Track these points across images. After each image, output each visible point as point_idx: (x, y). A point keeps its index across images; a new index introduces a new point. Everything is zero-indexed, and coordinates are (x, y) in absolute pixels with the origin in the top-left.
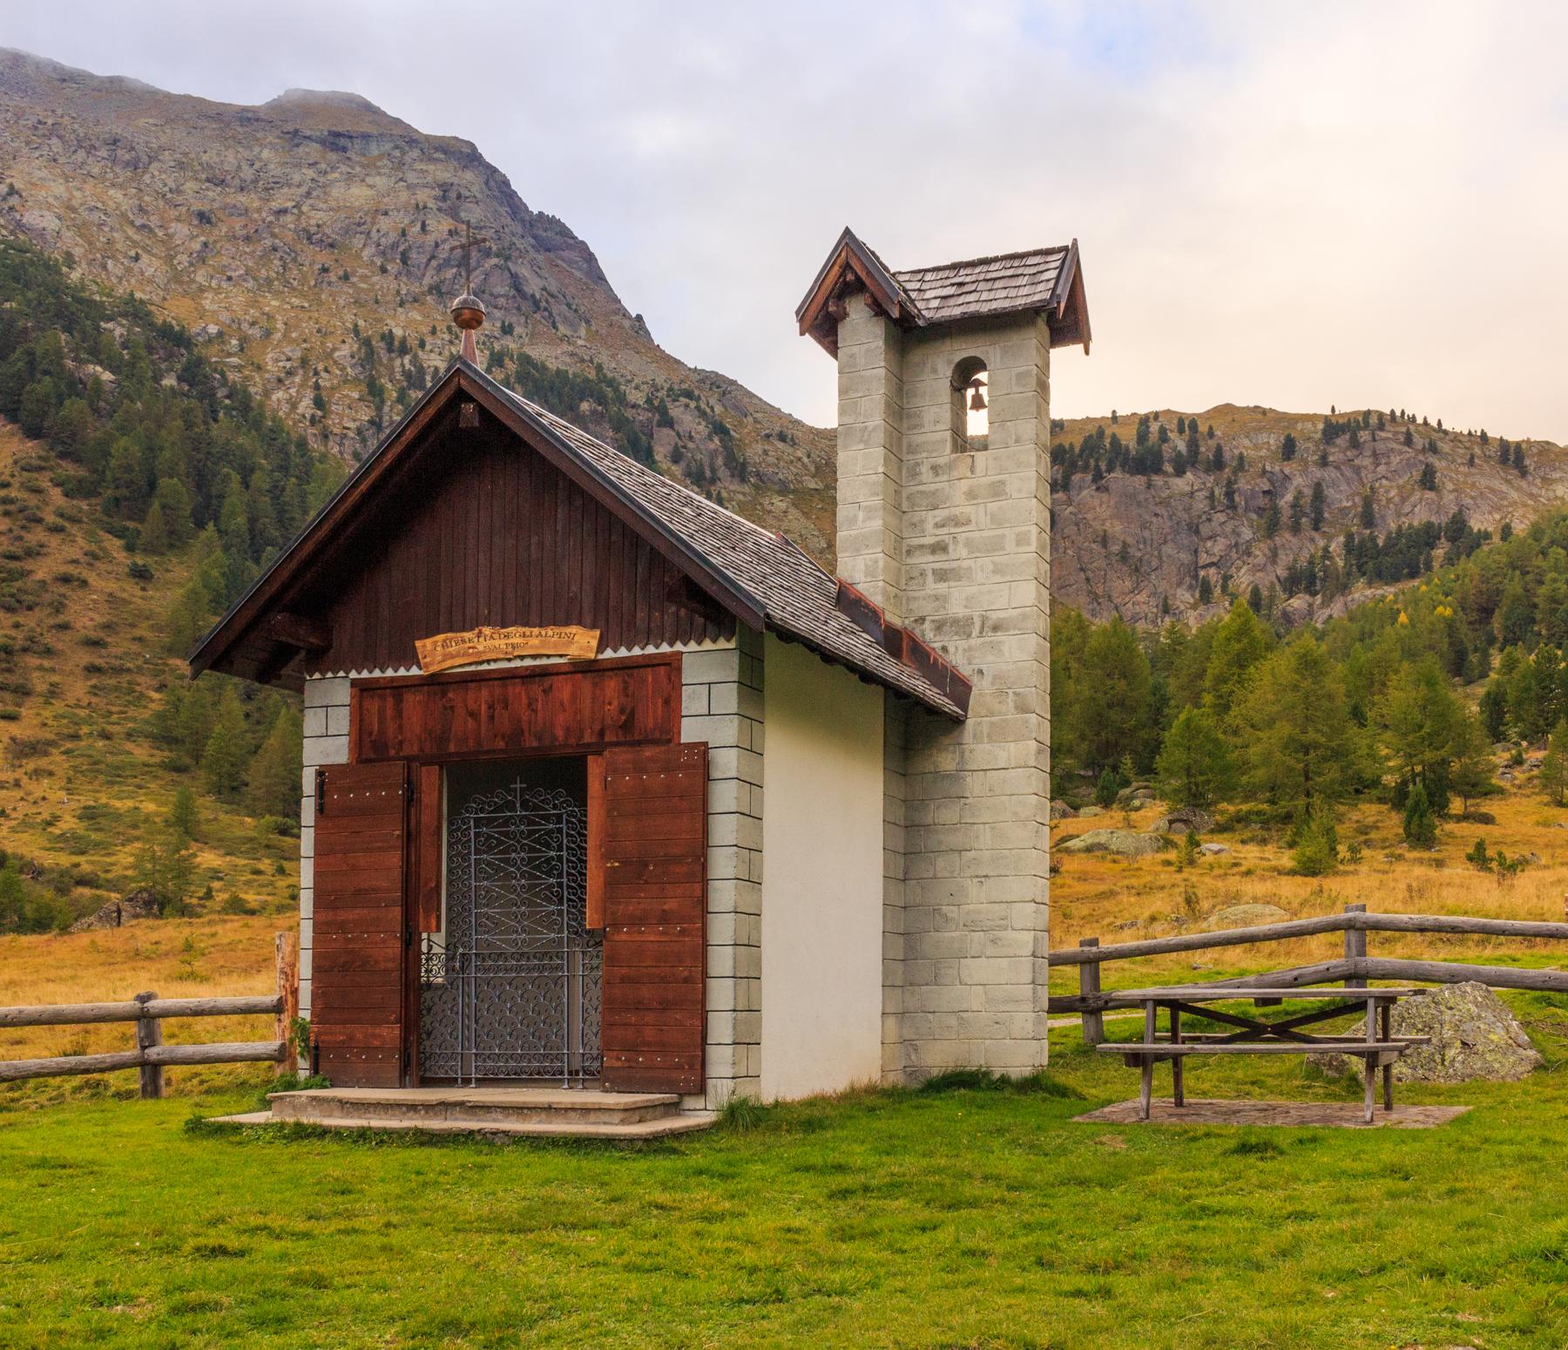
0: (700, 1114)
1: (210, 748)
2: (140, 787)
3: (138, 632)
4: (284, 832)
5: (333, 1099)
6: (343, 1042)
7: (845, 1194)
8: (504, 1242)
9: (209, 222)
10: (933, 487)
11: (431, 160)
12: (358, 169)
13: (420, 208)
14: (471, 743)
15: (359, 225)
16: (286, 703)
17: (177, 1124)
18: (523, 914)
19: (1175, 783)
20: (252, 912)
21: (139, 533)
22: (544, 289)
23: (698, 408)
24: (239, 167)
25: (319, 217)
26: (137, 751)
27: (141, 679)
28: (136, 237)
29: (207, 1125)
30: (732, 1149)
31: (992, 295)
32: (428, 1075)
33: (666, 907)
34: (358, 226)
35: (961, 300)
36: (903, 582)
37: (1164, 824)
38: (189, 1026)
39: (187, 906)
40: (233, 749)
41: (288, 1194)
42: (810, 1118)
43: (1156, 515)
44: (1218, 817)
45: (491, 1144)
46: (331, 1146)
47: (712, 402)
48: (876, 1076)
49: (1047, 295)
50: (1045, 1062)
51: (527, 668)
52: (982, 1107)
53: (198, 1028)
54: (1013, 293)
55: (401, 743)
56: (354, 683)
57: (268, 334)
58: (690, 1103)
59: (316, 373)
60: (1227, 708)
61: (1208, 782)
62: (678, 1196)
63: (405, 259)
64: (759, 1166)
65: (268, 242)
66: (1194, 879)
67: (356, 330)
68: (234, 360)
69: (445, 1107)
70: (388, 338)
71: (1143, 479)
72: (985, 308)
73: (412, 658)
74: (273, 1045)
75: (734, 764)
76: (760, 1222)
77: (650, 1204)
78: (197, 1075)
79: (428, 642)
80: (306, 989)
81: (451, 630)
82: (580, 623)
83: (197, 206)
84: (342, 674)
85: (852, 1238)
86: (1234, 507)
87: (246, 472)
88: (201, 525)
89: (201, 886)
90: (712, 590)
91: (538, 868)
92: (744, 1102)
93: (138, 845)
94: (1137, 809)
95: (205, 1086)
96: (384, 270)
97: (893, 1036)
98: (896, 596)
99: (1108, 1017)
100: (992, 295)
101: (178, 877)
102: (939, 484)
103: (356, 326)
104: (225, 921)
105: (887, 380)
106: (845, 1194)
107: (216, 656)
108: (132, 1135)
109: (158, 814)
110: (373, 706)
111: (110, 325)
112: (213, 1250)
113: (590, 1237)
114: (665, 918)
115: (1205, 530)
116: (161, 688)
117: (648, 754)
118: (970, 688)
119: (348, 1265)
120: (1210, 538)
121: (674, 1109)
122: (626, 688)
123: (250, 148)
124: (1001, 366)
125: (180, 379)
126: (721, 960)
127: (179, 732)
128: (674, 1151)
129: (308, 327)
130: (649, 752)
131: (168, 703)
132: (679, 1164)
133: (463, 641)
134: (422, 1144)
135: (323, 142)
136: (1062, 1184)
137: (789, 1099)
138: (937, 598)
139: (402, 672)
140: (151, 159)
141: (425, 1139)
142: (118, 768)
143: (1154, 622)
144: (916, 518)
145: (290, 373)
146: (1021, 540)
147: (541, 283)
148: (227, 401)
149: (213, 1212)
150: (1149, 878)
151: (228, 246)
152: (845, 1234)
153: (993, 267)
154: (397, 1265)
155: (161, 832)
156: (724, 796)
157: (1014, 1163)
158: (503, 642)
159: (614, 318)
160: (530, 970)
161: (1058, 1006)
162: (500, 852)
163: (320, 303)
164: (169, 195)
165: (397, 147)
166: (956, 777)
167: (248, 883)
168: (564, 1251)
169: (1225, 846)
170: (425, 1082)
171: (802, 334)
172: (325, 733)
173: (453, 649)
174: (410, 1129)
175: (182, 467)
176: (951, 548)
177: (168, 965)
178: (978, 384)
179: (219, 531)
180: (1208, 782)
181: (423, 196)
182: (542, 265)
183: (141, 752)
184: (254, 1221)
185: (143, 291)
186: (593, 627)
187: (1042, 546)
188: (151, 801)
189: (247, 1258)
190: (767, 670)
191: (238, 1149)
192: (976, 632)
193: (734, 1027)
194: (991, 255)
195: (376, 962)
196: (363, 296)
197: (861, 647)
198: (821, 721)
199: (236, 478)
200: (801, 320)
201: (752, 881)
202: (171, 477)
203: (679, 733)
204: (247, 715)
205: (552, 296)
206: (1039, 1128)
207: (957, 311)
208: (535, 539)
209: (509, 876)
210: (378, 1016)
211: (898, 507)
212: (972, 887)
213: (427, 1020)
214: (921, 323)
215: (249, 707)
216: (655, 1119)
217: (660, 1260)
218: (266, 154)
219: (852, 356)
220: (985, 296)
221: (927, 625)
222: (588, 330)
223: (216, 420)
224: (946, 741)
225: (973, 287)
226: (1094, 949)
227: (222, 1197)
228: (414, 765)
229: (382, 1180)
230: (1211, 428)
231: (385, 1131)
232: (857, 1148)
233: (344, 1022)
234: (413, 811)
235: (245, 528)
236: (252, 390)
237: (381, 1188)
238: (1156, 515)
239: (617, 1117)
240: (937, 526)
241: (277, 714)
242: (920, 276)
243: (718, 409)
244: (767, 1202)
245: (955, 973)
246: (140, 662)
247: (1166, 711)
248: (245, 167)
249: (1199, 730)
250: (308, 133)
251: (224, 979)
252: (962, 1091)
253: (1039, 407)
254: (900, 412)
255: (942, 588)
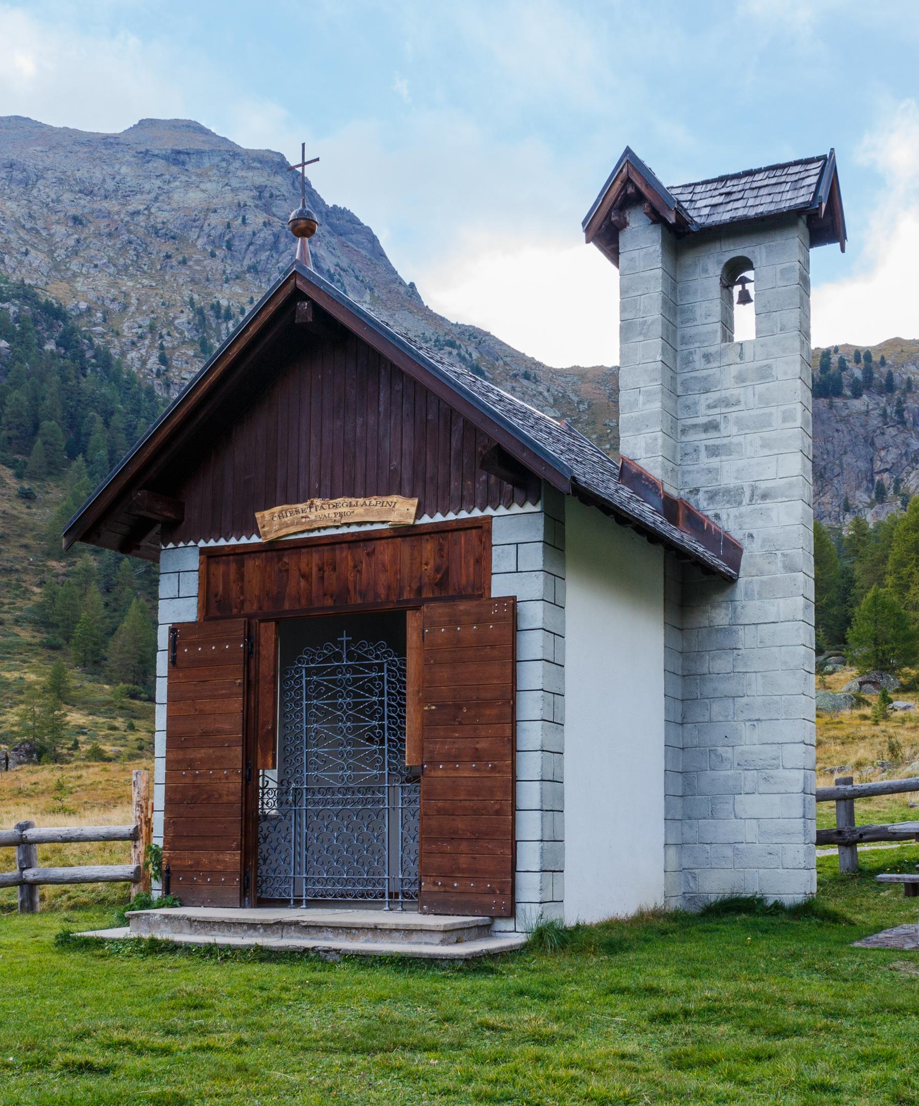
0: (510, 935)
1: (78, 632)
2: (24, 662)
3: (24, 541)
4: (134, 696)
5: (183, 917)
6: (191, 866)
7: (667, 1018)
8: (351, 1065)
9: (81, 223)
10: (704, 373)
11: (250, 168)
12: (194, 178)
13: (241, 206)
14: (303, 601)
15: (194, 221)
16: (136, 594)
17: (48, 937)
18: (349, 753)
19: (865, 650)
20: (109, 760)
21: (26, 463)
22: (337, 265)
23: (459, 355)
24: (104, 180)
25: (162, 216)
26: (23, 634)
27: (26, 578)
28: (27, 237)
29: (74, 939)
30: (544, 970)
31: (758, 201)
32: (264, 896)
33: (478, 746)
34: (194, 221)
35: (730, 206)
36: (679, 455)
37: (855, 685)
38: (60, 851)
39: (59, 755)
40: (95, 631)
41: (146, 1008)
42: (610, 940)
43: (837, 431)
44: (902, 679)
45: (324, 961)
46: (182, 960)
47: (470, 349)
48: (660, 902)
49: (810, 198)
50: (815, 890)
51: (353, 534)
52: (766, 931)
53: (67, 852)
54: (777, 198)
55: (242, 602)
56: (203, 551)
57: (125, 307)
58: (501, 925)
59: (161, 337)
60: (907, 587)
61: (893, 649)
62: (506, 1016)
63: (229, 247)
64: (574, 987)
65: (125, 237)
66: (891, 731)
67: (192, 302)
68: (99, 329)
69: (281, 926)
70: (216, 308)
71: (826, 401)
72: (752, 213)
73: (252, 527)
74: (126, 869)
75: (540, 615)
76: (591, 1047)
77: (482, 1024)
78: (66, 892)
79: (267, 513)
80: (159, 820)
81: (286, 503)
82: (400, 493)
83: (72, 211)
84: (192, 543)
85: (690, 1067)
86: (903, 422)
87: (107, 415)
88: (72, 456)
89: (70, 739)
90: (523, 457)
91: (361, 712)
92: (552, 924)
93: (23, 706)
94: (831, 673)
95: (72, 902)
96: (213, 255)
97: (673, 866)
98: (673, 470)
99: (861, 848)
100: (758, 201)
101: (52, 732)
102: (712, 369)
103: (192, 299)
104: (88, 767)
105: (664, 279)
106: (667, 1018)
107: (87, 529)
108: (10, 947)
109: (37, 683)
110: (219, 570)
111: (6, 305)
112: (80, 1066)
113: (432, 1060)
114: (477, 756)
115: (879, 442)
116: (41, 584)
117: (462, 608)
118: (741, 551)
119: (207, 1086)
120: (884, 448)
121: (485, 931)
122: (441, 550)
123: (112, 166)
124: (770, 261)
125: (58, 344)
126: (529, 795)
127: (55, 619)
128: (492, 971)
129: (155, 301)
130: (463, 606)
131: (46, 595)
132: (499, 983)
133: (297, 512)
134: (262, 960)
135: (166, 158)
136: (877, 1011)
137: (588, 923)
138: (709, 471)
139: (244, 540)
140: (38, 178)
141: (264, 955)
142: (9, 647)
143: (837, 519)
144: (689, 400)
145: (141, 337)
146: (787, 417)
147: (335, 260)
148: (93, 361)
149: (79, 1025)
150: (852, 730)
151: (95, 241)
152: (680, 1063)
153: (758, 177)
154: (253, 1087)
155: (39, 696)
156: (532, 645)
157: (818, 989)
158: (332, 511)
159: (393, 286)
160: (354, 803)
161: (823, 839)
162: (328, 698)
163: (164, 282)
164: (51, 204)
165: (224, 160)
166: (729, 630)
167: (106, 737)
168: (414, 1077)
169: (910, 703)
170: (262, 903)
171: (588, 242)
172: (178, 602)
173: (288, 519)
174: (251, 946)
175: (59, 413)
176: (722, 427)
177: (43, 802)
178: (744, 281)
179: (86, 461)
180: (893, 649)
181: (243, 197)
182: (336, 247)
183: (26, 635)
184: (118, 1036)
185: (31, 278)
186: (412, 496)
187: (805, 421)
188: (33, 672)
189: (112, 1076)
190: (567, 528)
191: (101, 962)
192: (746, 500)
193: (542, 856)
194: (755, 167)
195: (220, 796)
196: (197, 275)
197: (647, 511)
198: (614, 576)
199: (99, 419)
200: (587, 231)
201: (555, 722)
202: (51, 420)
203: (490, 588)
204: (107, 605)
205: (344, 270)
206: (830, 953)
207: (726, 217)
208: (360, 421)
209: (337, 719)
210: (223, 843)
211: (673, 391)
212: (745, 730)
213: (264, 847)
214: (694, 228)
215: (109, 598)
216: (470, 940)
217: (509, 1088)
218: (124, 170)
219: (632, 259)
220: (751, 202)
221: (701, 496)
222: (372, 296)
223: (85, 375)
224: (719, 598)
225: (740, 195)
226: (849, 787)
227: (88, 1010)
228: (255, 621)
229: (230, 995)
230: (883, 358)
231: (229, 947)
232: (664, 972)
233: (192, 849)
234: (252, 663)
235: (106, 458)
236: (112, 351)
237: (229, 1004)
238: (837, 431)
239: (438, 938)
240: (709, 407)
241: (130, 603)
242: (690, 189)
243: (475, 355)
244: (592, 1025)
245: (731, 807)
246: (25, 564)
247: (853, 591)
248: (109, 180)
249: (884, 606)
250: (156, 152)
251: (88, 813)
252: (744, 916)
253: (801, 298)
254: (675, 307)
255: (714, 462)
